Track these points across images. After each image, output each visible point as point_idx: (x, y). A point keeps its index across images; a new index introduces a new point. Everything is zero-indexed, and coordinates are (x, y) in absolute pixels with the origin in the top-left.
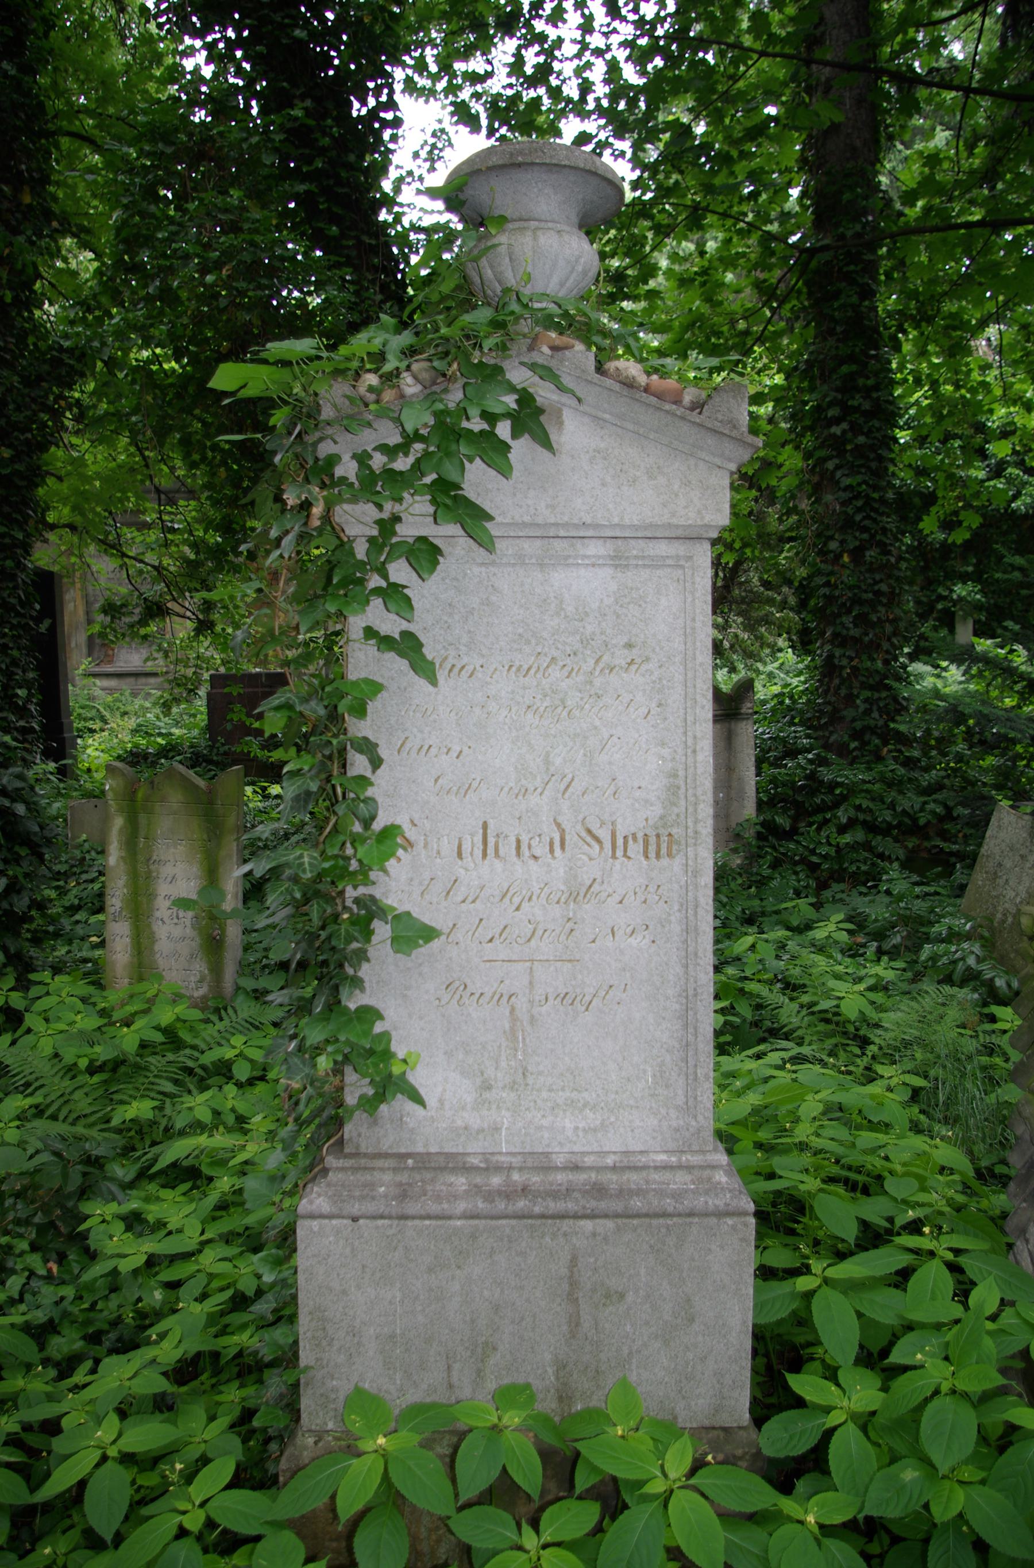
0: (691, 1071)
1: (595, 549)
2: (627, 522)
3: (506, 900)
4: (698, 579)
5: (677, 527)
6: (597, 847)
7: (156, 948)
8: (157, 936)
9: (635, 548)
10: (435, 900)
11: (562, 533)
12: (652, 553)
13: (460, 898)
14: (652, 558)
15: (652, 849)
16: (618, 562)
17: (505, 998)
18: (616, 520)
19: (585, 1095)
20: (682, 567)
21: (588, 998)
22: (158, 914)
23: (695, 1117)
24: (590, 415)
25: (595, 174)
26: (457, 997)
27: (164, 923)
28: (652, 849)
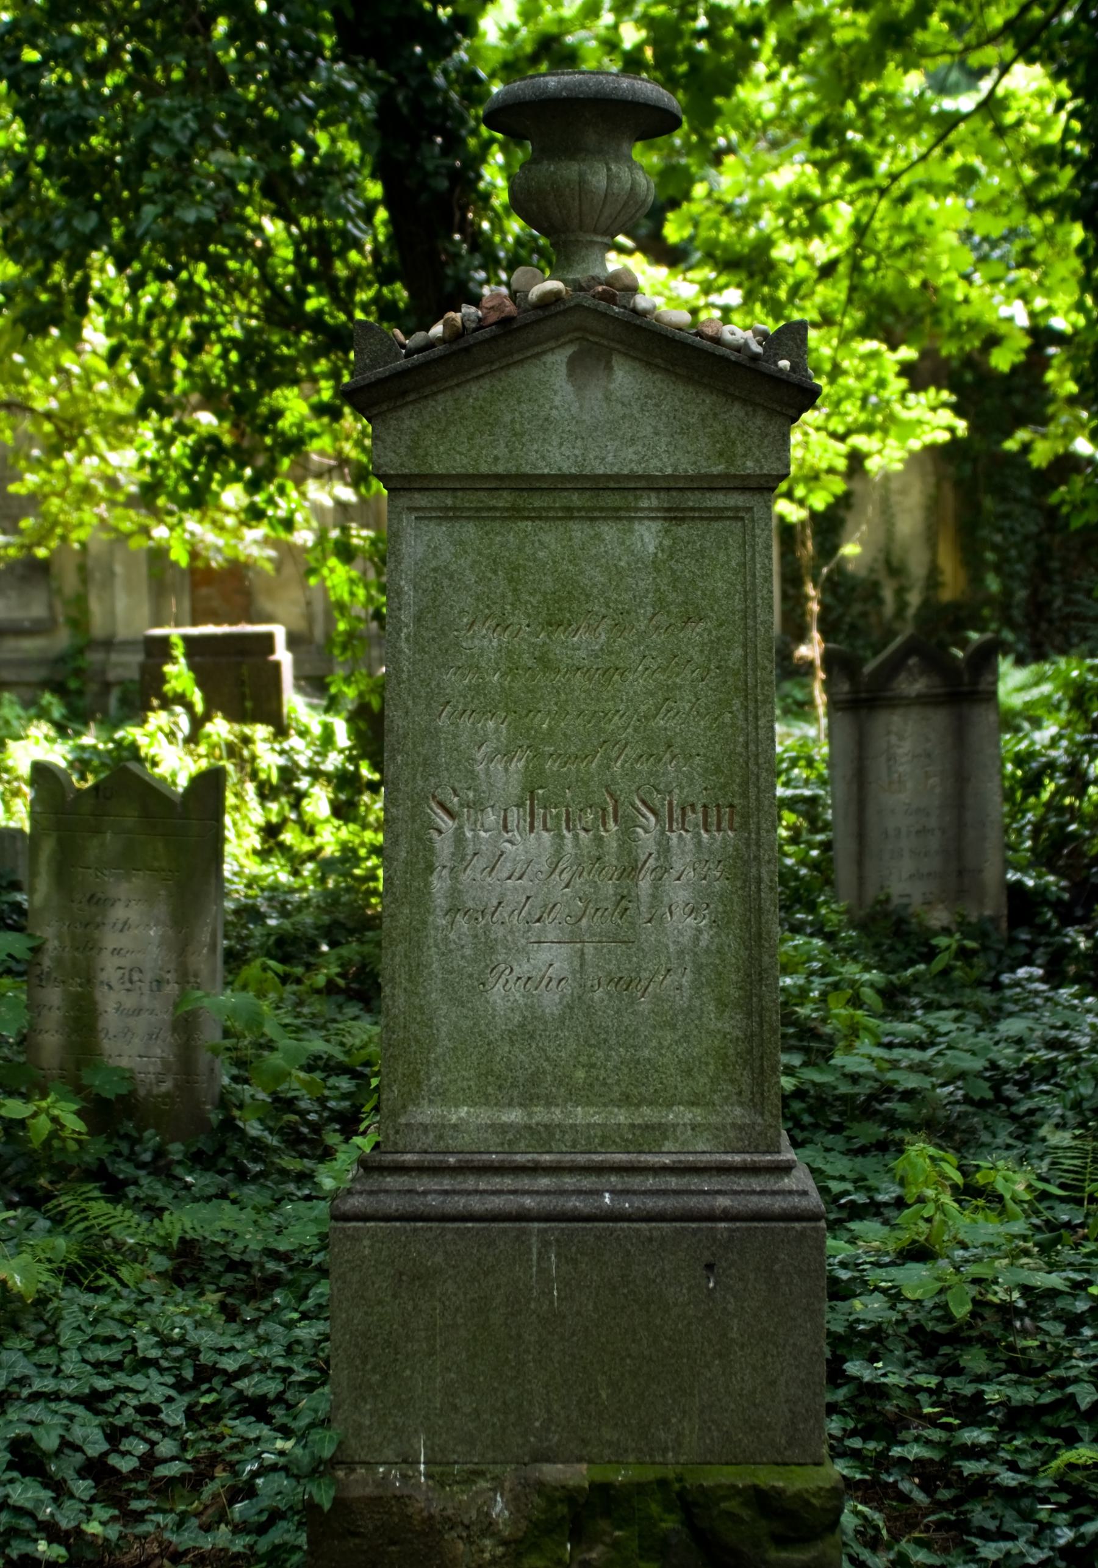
0: (757, 1063)
1: (650, 501)
2: (681, 472)
3: (556, 876)
4: (758, 532)
5: (735, 476)
6: (652, 819)
7: (101, 1025)
8: (101, 1008)
9: (692, 500)
10: (478, 877)
11: (612, 485)
12: (709, 504)
13: (506, 875)
14: (709, 510)
15: (713, 819)
16: (674, 516)
17: (554, 983)
18: (669, 471)
19: (643, 1089)
20: (742, 519)
21: (644, 983)
22: (103, 976)
23: (762, 1114)
24: (735, 489)
25: (639, 328)
26: (502, 981)
27: (110, 987)
28: (713, 819)
